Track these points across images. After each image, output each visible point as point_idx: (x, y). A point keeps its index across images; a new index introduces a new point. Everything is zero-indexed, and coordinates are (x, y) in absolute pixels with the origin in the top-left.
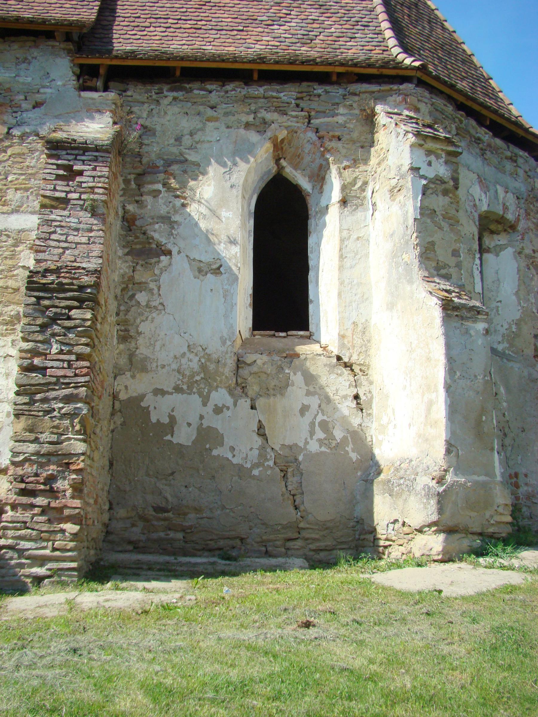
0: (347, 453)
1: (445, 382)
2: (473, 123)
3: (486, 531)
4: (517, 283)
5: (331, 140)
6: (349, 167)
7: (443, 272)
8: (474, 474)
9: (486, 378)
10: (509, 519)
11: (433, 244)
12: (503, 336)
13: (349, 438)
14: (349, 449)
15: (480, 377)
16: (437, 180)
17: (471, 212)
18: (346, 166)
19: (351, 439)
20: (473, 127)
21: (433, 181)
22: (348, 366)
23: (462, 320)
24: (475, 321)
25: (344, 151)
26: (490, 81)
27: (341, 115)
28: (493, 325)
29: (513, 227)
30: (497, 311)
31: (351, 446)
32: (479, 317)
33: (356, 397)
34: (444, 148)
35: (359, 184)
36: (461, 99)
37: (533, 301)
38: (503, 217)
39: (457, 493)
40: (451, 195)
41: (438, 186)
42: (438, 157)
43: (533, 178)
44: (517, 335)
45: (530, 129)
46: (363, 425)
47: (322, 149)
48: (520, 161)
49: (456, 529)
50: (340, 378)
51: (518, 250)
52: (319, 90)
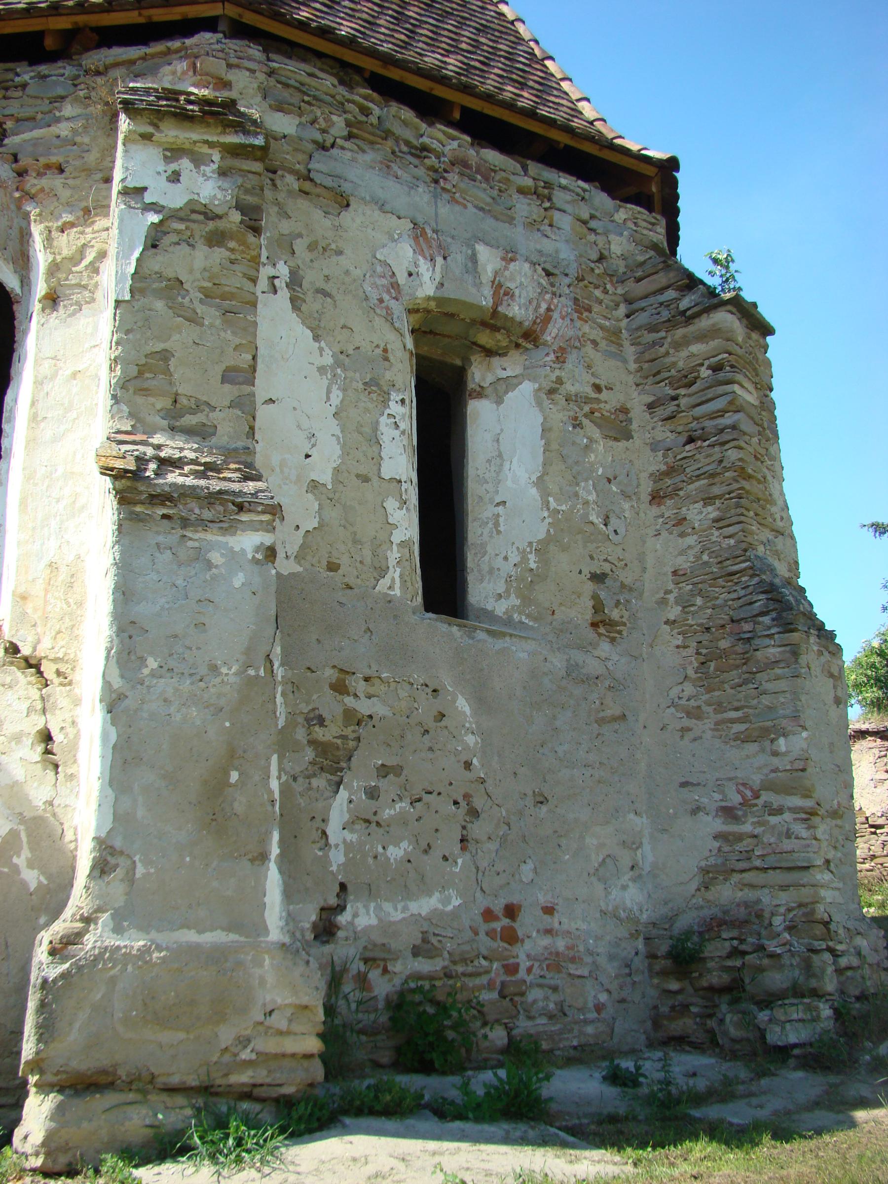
0: (16, 870)
1: (107, 684)
2: (407, 114)
3: (218, 1082)
4: (541, 459)
5: (40, 175)
6: (72, 225)
7: (190, 420)
8: (182, 926)
9: (252, 672)
10: (314, 1045)
11: (165, 356)
12: (509, 579)
13: (23, 836)
14: (20, 861)
15: (230, 672)
16: (193, 211)
17: (381, 301)
18: (65, 224)
19: (29, 836)
20: (405, 123)
21: (182, 214)
22: (33, 665)
23: (184, 527)
24: (231, 528)
25: (64, 194)
26: (548, 63)
27: (68, 119)
28: (486, 558)
29: (529, 337)
30: (497, 525)
31: (26, 853)
32: (244, 517)
33: (47, 737)
34: (215, 139)
35: (90, 256)
36: (370, 65)
37: (592, 497)
38: (495, 313)
39: (113, 981)
40: (232, 244)
41: (194, 226)
42: (198, 161)
43: (606, 234)
44: (538, 577)
45: (616, 141)
46: (56, 803)
47: (17, 195)
48: (560, 197)
49: (103, 1079)
50: (10, 693)
51: (547, 385)
52: (26, 74)
